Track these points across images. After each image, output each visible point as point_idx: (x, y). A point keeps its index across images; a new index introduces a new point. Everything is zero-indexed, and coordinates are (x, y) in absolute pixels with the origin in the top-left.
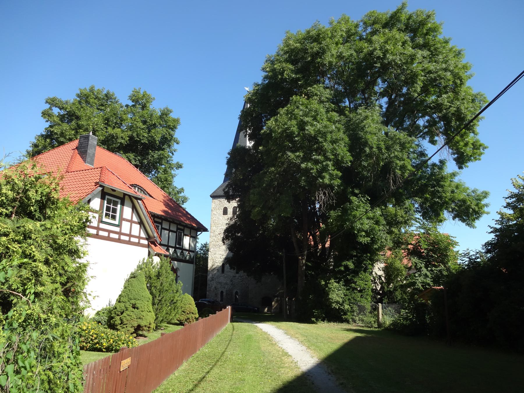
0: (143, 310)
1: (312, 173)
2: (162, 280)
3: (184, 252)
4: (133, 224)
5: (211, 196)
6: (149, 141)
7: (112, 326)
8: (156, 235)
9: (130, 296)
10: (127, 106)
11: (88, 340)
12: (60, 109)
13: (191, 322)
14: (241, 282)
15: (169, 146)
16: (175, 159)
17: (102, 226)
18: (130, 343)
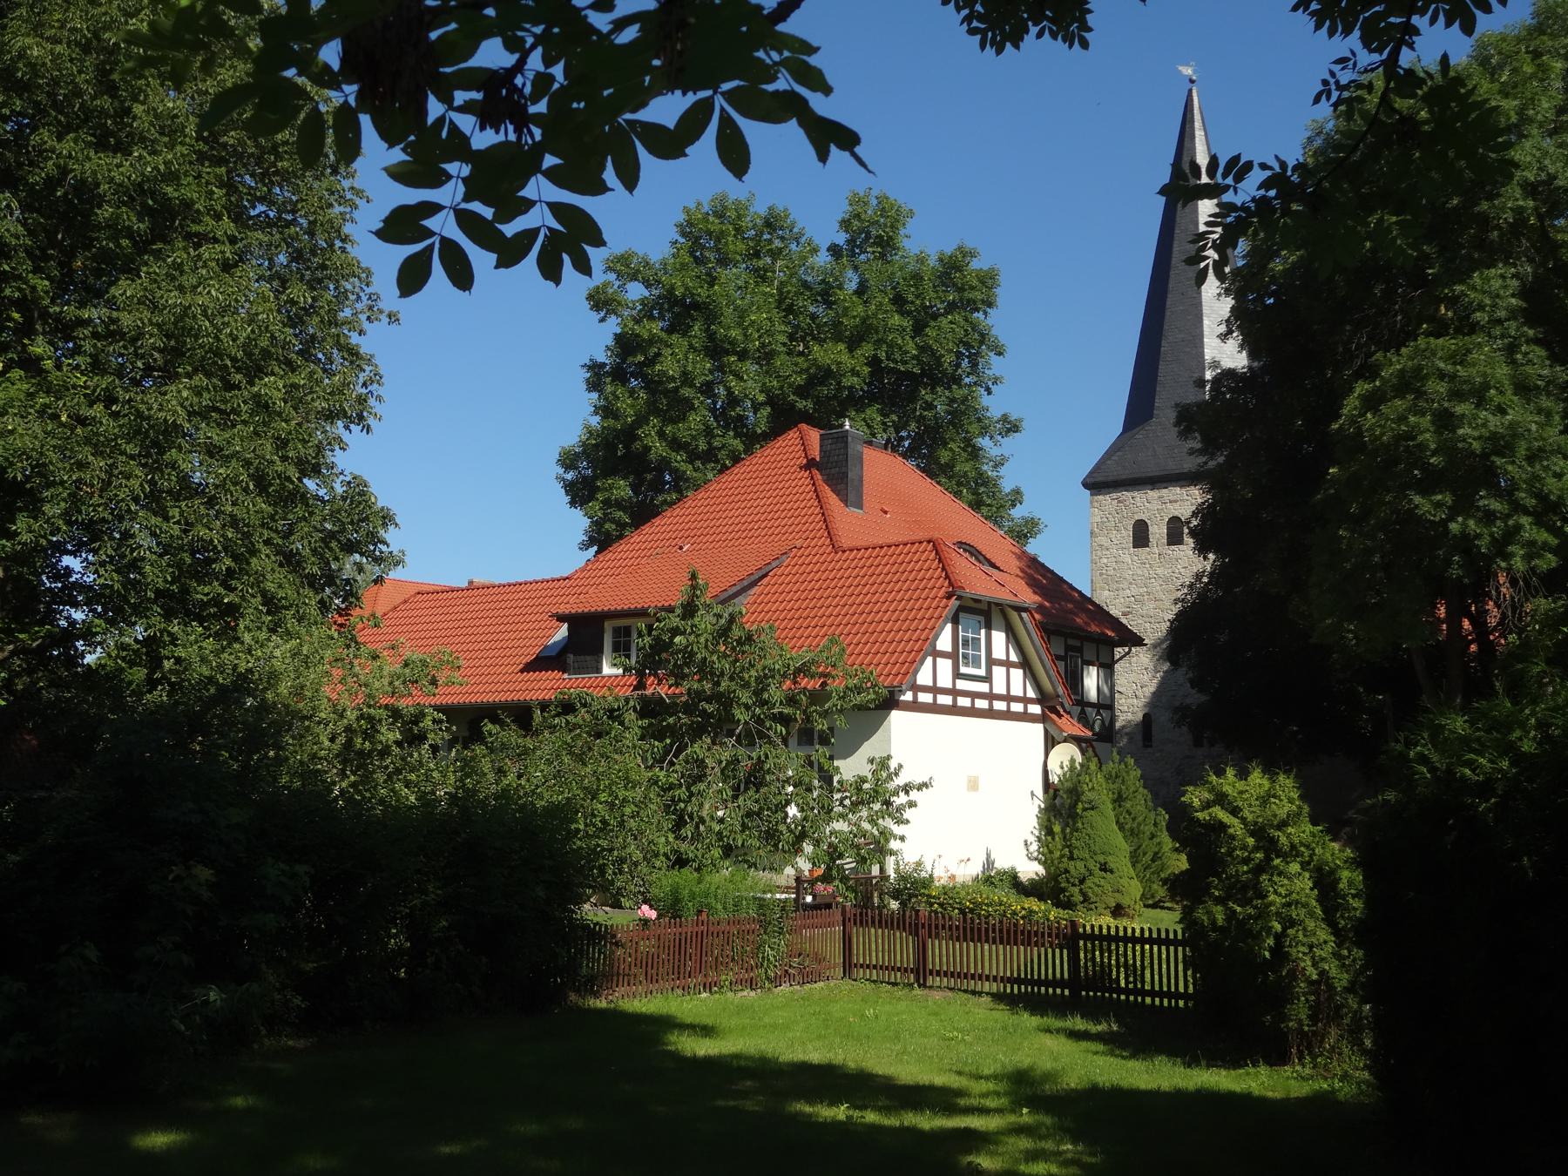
1: (1478, 547)
3: (1089, 710)
5: (1086, 485)
16: (994, 405)
17: (962, 685)
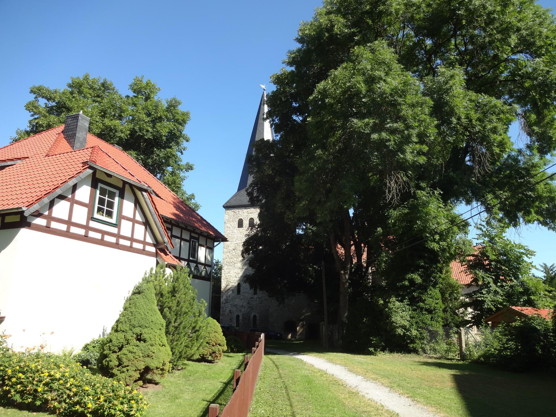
0: (153, 342)
2: (179, 297)
3: (199, 266)
4: (136, 225)
5: (224, 207)
6: (154, 136)
7: (106, 371)
8: (166, 239)
9: (133, 322)
10: (128, 97)
11: (62, 397)
12: (48, 100)
13: (217, 357)
14: (260, 304)
15: (178, 144)
16: (184, 159)
17: (93, 224)
18: (133, 402)
